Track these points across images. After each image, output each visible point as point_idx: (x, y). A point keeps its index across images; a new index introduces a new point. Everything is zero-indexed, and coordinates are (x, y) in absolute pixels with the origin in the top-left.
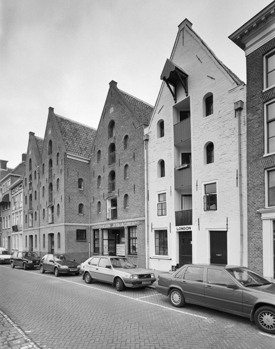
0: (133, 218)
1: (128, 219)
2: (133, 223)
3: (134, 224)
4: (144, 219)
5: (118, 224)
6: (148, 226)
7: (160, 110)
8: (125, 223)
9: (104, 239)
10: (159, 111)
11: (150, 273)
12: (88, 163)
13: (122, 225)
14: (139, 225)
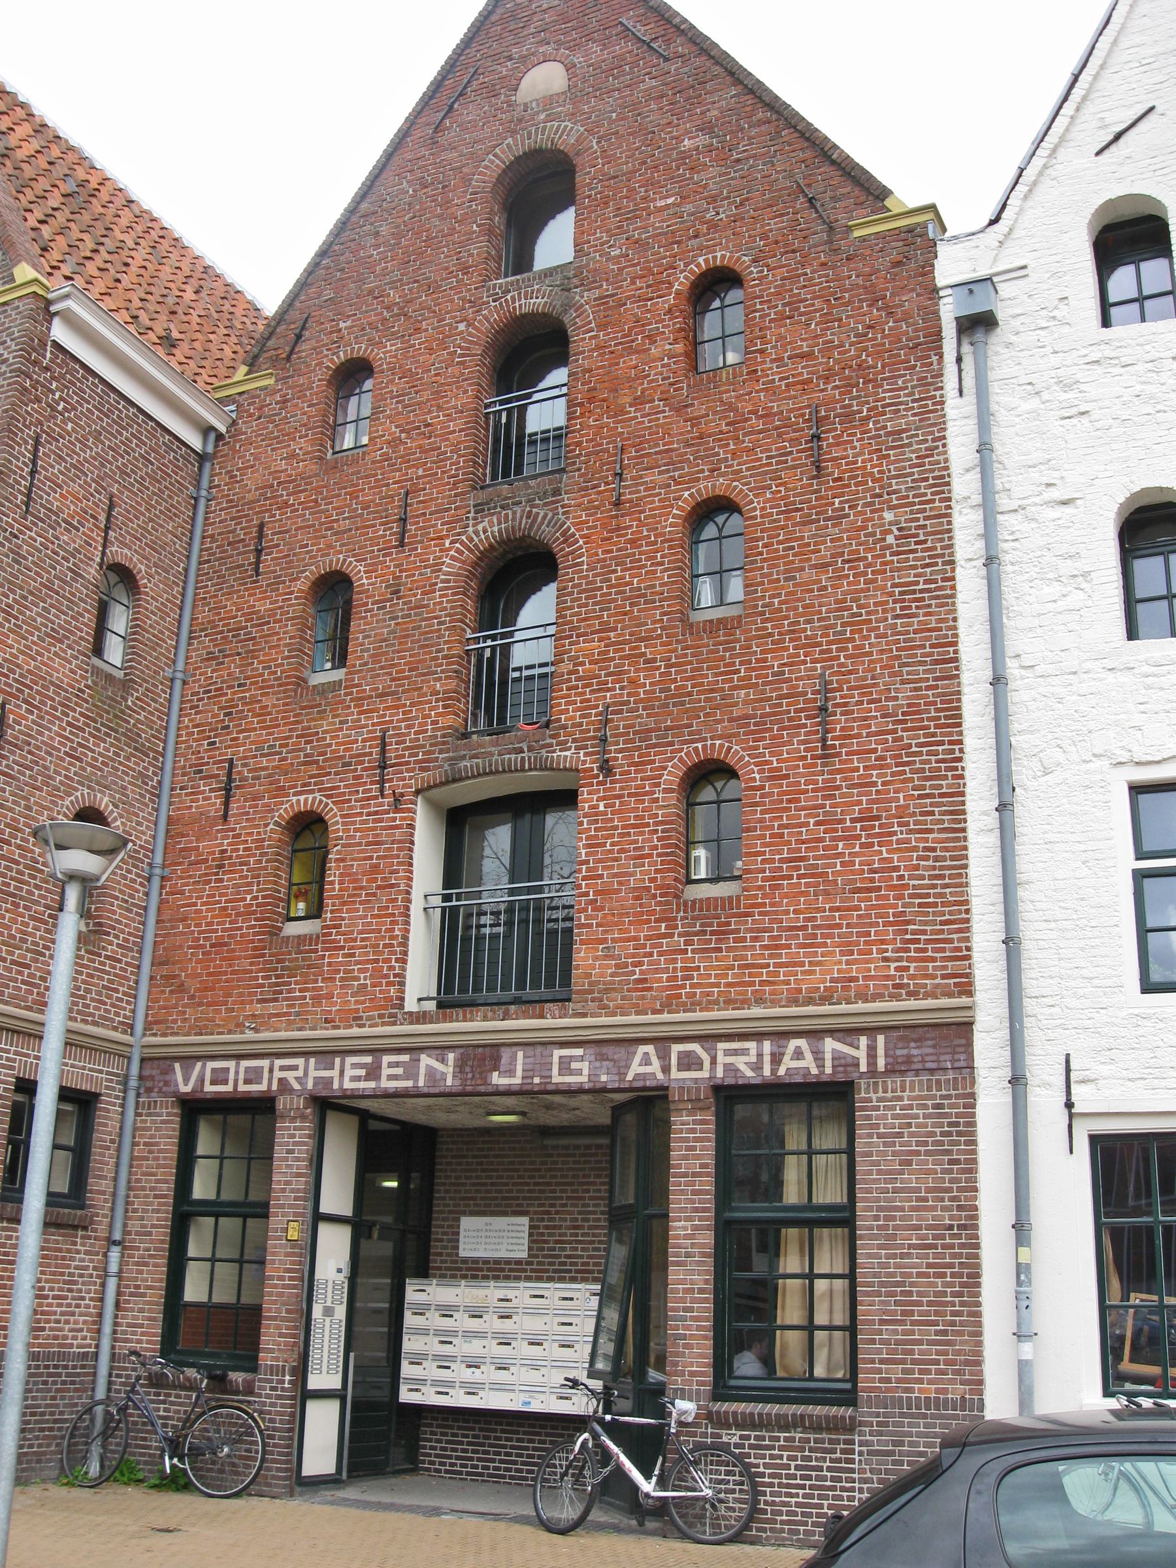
0: (795, 1002)
1: (729, 1003)
3: (808, 1062)
4: (959, 1016)
5: (579, 1052)
7: (1118, 137)
8: (676, 1048)
9: (324, 1209)
10: (1111, 137)
12: (202, 458)
13: (643, 1066)
14: (890, 1071)
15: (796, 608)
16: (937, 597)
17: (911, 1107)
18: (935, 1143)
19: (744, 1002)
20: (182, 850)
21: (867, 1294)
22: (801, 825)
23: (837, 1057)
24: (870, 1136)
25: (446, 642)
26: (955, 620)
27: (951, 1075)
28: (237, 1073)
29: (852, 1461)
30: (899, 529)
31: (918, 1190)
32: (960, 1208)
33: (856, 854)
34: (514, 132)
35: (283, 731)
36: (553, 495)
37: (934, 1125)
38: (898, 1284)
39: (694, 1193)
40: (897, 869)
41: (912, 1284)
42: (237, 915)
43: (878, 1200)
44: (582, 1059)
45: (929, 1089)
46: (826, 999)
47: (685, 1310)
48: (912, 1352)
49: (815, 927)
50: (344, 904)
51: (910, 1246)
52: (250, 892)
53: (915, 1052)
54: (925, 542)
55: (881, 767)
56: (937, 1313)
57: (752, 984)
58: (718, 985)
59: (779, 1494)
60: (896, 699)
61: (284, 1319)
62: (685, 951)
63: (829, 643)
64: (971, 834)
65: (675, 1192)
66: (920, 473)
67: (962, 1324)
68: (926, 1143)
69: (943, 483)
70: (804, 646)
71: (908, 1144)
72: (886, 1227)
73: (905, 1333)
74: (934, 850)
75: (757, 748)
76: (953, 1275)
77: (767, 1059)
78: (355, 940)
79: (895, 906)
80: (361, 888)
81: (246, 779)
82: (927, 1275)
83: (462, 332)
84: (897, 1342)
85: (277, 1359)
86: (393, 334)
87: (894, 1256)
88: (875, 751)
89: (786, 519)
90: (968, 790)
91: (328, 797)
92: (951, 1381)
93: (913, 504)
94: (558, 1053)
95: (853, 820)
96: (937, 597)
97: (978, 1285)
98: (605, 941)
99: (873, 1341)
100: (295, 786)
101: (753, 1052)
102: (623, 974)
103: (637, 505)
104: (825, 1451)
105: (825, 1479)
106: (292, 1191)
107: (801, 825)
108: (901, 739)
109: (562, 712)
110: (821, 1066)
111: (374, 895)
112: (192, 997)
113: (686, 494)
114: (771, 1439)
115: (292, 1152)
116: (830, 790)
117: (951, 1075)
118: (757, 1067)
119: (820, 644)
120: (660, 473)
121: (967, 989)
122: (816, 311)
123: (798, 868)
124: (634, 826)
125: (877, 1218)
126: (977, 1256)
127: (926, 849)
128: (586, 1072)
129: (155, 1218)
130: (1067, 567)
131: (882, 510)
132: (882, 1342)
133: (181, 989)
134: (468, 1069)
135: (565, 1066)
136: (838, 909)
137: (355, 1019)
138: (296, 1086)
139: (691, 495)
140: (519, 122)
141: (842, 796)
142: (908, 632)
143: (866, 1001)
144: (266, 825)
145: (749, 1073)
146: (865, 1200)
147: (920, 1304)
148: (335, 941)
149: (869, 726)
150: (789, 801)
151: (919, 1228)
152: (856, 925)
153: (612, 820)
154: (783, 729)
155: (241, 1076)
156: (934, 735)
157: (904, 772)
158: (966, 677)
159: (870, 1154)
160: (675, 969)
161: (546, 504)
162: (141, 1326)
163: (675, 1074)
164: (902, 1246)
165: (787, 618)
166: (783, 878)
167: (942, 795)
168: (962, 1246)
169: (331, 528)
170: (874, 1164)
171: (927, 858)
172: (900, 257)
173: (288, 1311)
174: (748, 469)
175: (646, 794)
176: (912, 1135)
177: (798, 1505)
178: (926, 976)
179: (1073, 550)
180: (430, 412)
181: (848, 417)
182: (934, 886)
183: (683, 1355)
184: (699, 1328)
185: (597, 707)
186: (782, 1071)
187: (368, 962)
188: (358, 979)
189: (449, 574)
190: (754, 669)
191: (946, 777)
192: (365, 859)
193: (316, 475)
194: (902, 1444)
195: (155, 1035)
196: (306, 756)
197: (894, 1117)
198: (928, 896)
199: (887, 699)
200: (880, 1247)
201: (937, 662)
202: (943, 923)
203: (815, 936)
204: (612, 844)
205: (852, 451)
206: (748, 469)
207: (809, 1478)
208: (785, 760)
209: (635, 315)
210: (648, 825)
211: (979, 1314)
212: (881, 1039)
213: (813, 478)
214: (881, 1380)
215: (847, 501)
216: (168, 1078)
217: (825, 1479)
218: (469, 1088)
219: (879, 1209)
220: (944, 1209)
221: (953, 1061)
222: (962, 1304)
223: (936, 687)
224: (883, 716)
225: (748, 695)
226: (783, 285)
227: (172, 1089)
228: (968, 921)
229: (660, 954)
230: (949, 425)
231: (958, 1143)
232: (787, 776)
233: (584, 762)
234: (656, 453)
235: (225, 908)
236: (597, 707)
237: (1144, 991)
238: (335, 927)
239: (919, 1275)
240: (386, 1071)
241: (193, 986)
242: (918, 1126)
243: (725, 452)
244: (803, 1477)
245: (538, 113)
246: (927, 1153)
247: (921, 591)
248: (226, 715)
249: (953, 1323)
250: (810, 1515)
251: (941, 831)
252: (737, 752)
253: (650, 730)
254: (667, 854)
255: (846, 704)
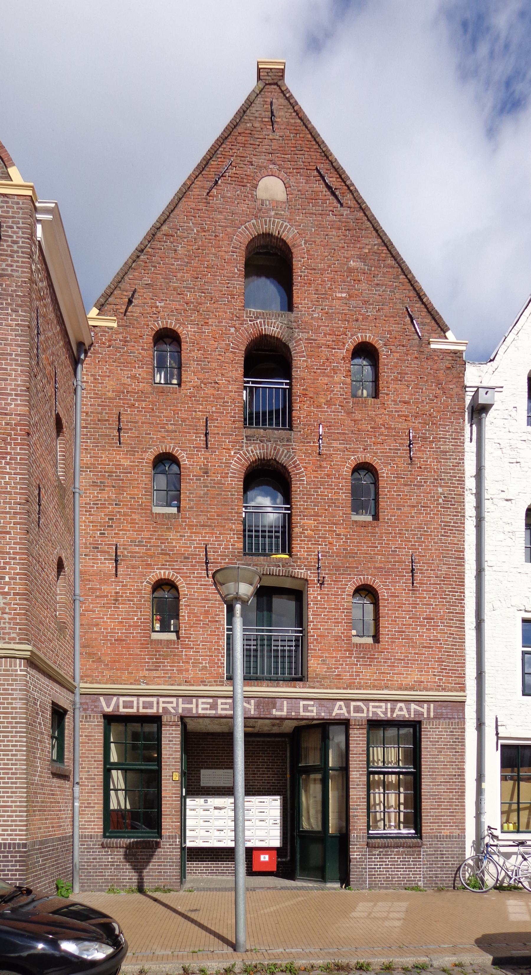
0: (400, 689)
1: (375, 687)
2: (401, 709)
3: (405, 713)
5: (312, 703)
6: (480, 725)
8: (353, 704)
11: (236, 793)
13: (339, 711)
14: (435, 718)
15: (402, 524)
16: (458, 530)
17: (442, 732)
18: (450, 745)
19: (381, 687)
20: (90, 589)
21: (426, 799)
22: (403, 618)
23: (416, 711)
24: (427, 741)
25: (236, 505)
26: (464, 541)
27: (457, 720)
28: (138, 703)
29: (420, 858)
30: (445, 497)
31: (444, 762)
32: (458, 769)
33: (424, 633)
34: (256, 217)
35: (146, 534)
36: (287, 441)
37: (450, 739)
38: (436, 795)
39: (360, 761)
40: (439, 640)
41: (441, 795)
42: (129, 626)
43: (430, 765)
44: (313, 706)
45: (449, 725)
46: (412, 689)
47: (357, 805)
48: (441, 819)
49: (408, 660)
50: (191, 627)
51: (441, 782)
52: (137, 615)
53: (444, 711)
54: (454, 505)
55: (435, 598)
56: (450, 806)
57: (384, 680)
58: (370, 680)
59: (394, 871)
60: (441, 571)
61: (173, 815)
62: (357, 665)
63: (415, 542)
64: (466, 629)
65: (352, 761)
66: (453, 473)
67: (459, 809)
68: (447, 745)
69: (462, 480)
70: (405, 541)
71: (441, 745)
72: (433, 775)
73: (439, 812)
74: (453, 634)
75: (386, 582)
76: (456, 792)
77: (389, 710)
78: (199, 645)
79: (438, 655)
80: (200, 620)
81: (127, 556)
82: (446, 792)
83: (232, 334)
84: (436, 816)
85: (172, 832)
86: (191, 321)
87: (435, 785)
88: (432, 591)
89: (398, 481)
90: (466, 613)
91: (177, 573)
92: (455, 829)
93: (450, 487)
94: (302, 703)
95: (424, 619)
96: (458, 530)
97: (464, 796)
98: (322, 657)
99: (428, 816)
100: (158, 565)
101: (384, 707)
102: (330, 672)
103: (329, 457)
104: (410, 855)
105: (411, 865)
106: (173, 758)
107: (403, 618)
108: (442, 588)
109: (298, 551)
110: (410, 714)
111: (208, 625)
112: (107, 665)
113: (353, 458)
114: (391, 851)
115: (172, 741)
116: (415, 605)
117: (457, 720)
118: (385, 713)
119: (411, 542)
120: (340, 444)
121: (463, 689)
122: (412, 381)
123: (402, 635)
124: (334, 609)
125: (429, 772)
126: (464, 786)
127: (450, 634)
128: (315, 711)
129: (98, 772)
130: (507, 528)
131: (437, 486)
132: (431, 816)
133: (99, 660)
134: (261, 707)
135: (306, 708)
136: (417, 654)
137: (202, 682)
138: (173, 711)
139: (355, 458)
140: (259, 210)
141: (420, 608)
142: (446, 543)
143: (427, 691)
144: (142, 582)
145: (382, 715)
146: (425, 765)
147: (444, 802)
148: (188, 644)
149: (430, 580)
150: (399, 607)
151: (444, 775)
152: (424, 661)
153: (324, 605)
154: (397, 576)
155: (141, 705)
156: (454, 588)
157: (443, 602)
158: (467, 566)
159: (427, 748)
160: (352, 672)
161: (283, 445)
162: (94, 821)
163: (352, 714)
164: (438, 782)
165: (398, 527)
166: (396, 639)
167: (457, 613)
168: (459, 782)
169: (164, 428)
170: (428, 752)
171: (450, 637)
172: (450, 366)
173: (175, 811)
174: (381, 452)
175: (339, 595)
176: (442, 742)
177: (401, 874)
178: (449, 683)
179: (509, 522)
180: (217, 375)
181: (425, 439)
182: (453, 649)
183: (357, 822)
184: (362, 812)
185: (314, 552)
186: (395, 715)
187: (207, 656)
188: (202, 663)
189: (235, 470)
190: (384, 547)
191: (458, 606)
192: (201, 607)
193: (151, 393)
194: (438, 851)
195: (86, 682)
196: (162, 550)
197: (436, 735)
198: (450, 652)
199: (438, 570)
200: (430, 782)
201: (456, 558)
202: (455, 663)
203: (408, 663)
204: (324, 615)
205: (425, 455)
206: (381, 452)
207: (405, 865)
208: (397, 589)
209: (326, 355)
210: (340, 609)
211: (464, 806)
212: (432, 705)
213: (409, 464)
214: (430, 829)
215: (423, 479)
216: (96, 704)
217: (411, 865)
218: (262, 716)
219: (430, 768)
220: (453, 769)
221: (458, 715)
222: (459, 802)
223: (456, 568)
224: (436, 577)
225: (381, 558)
226: (397, 363)
227: (100, 710)
228: (464, 663)
229: (346, 665)
230: (466, 454)
231: (458, 745)
232: (398, 596)
233: (310, 577)
234: (338, 433)
235: (122, 622)
236: (314, 552)
237: (523, 695)
238: (187, 638)
239: (444, 792)
240: (220, 707)
241: (107, 659)
242: (444, 738)
243: (370, 442)
244: (403, 865)
245: (270, 210)
246: (447, 749)
247: (452, 526)
248: (109, 519)
249: (455, 809)
250: (405, 878)
251: (456, 627)
252: (377, 583)
253: (340, 567)
254: (349, 623)
255: (421, 570)
